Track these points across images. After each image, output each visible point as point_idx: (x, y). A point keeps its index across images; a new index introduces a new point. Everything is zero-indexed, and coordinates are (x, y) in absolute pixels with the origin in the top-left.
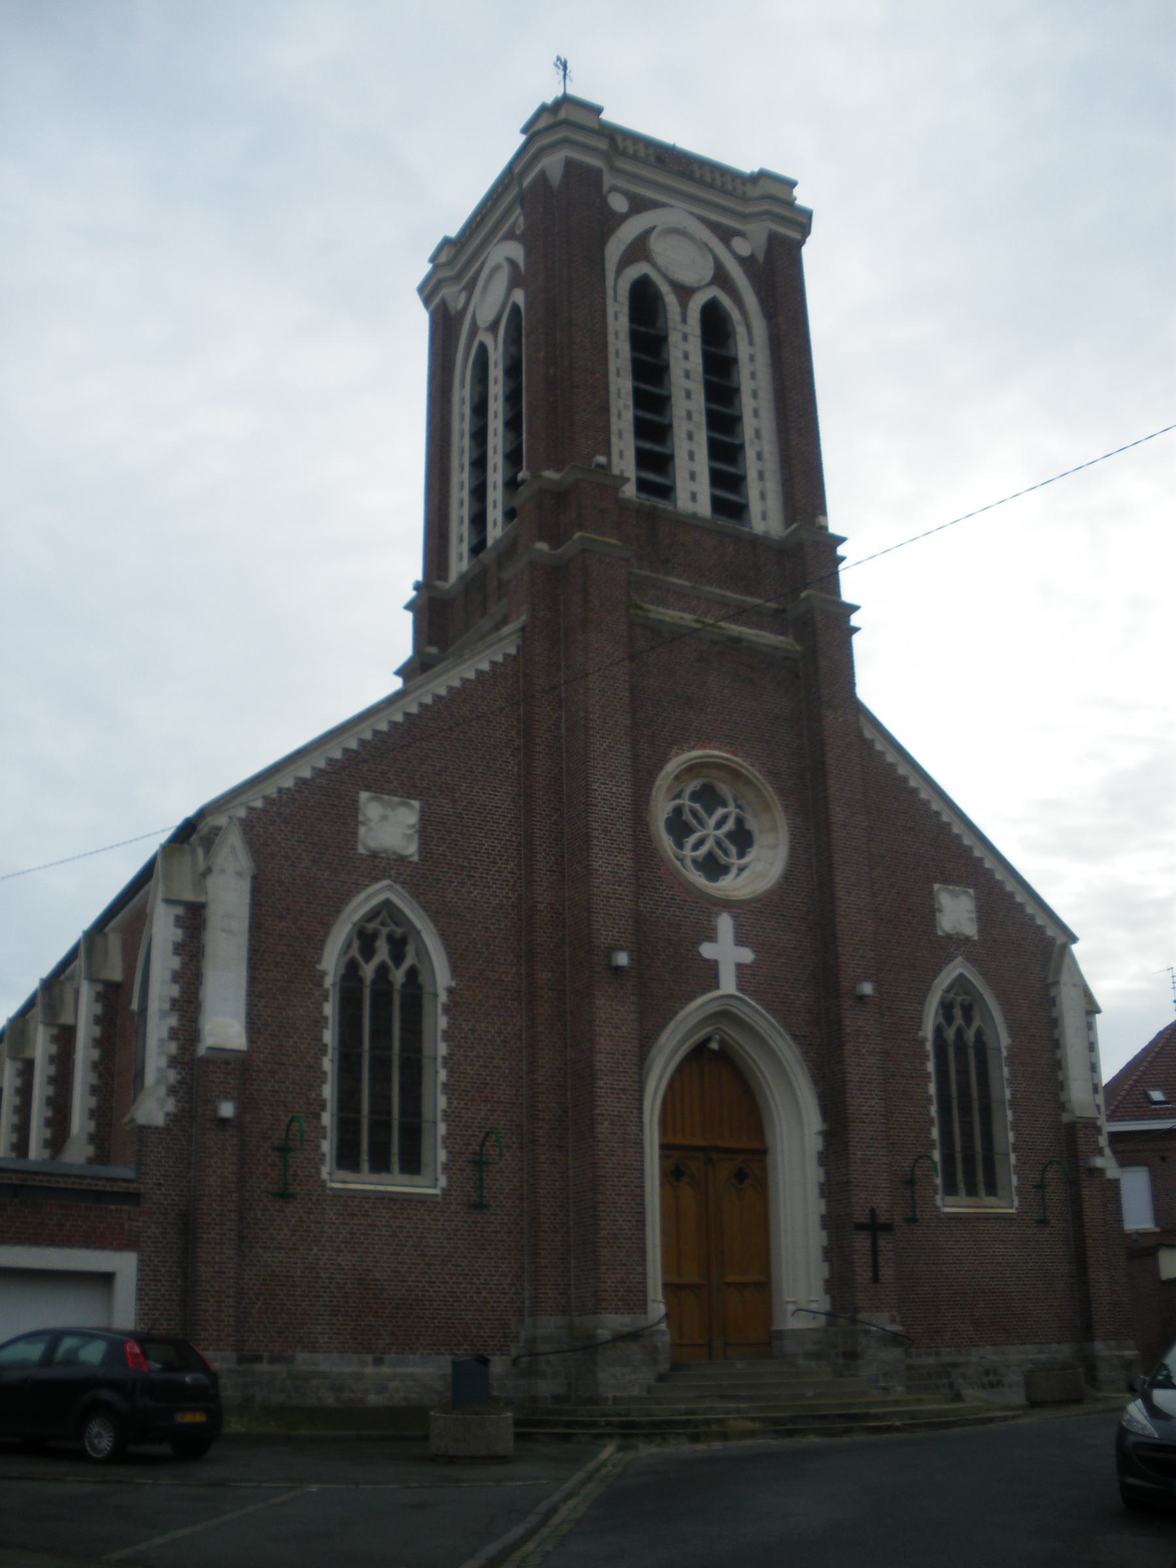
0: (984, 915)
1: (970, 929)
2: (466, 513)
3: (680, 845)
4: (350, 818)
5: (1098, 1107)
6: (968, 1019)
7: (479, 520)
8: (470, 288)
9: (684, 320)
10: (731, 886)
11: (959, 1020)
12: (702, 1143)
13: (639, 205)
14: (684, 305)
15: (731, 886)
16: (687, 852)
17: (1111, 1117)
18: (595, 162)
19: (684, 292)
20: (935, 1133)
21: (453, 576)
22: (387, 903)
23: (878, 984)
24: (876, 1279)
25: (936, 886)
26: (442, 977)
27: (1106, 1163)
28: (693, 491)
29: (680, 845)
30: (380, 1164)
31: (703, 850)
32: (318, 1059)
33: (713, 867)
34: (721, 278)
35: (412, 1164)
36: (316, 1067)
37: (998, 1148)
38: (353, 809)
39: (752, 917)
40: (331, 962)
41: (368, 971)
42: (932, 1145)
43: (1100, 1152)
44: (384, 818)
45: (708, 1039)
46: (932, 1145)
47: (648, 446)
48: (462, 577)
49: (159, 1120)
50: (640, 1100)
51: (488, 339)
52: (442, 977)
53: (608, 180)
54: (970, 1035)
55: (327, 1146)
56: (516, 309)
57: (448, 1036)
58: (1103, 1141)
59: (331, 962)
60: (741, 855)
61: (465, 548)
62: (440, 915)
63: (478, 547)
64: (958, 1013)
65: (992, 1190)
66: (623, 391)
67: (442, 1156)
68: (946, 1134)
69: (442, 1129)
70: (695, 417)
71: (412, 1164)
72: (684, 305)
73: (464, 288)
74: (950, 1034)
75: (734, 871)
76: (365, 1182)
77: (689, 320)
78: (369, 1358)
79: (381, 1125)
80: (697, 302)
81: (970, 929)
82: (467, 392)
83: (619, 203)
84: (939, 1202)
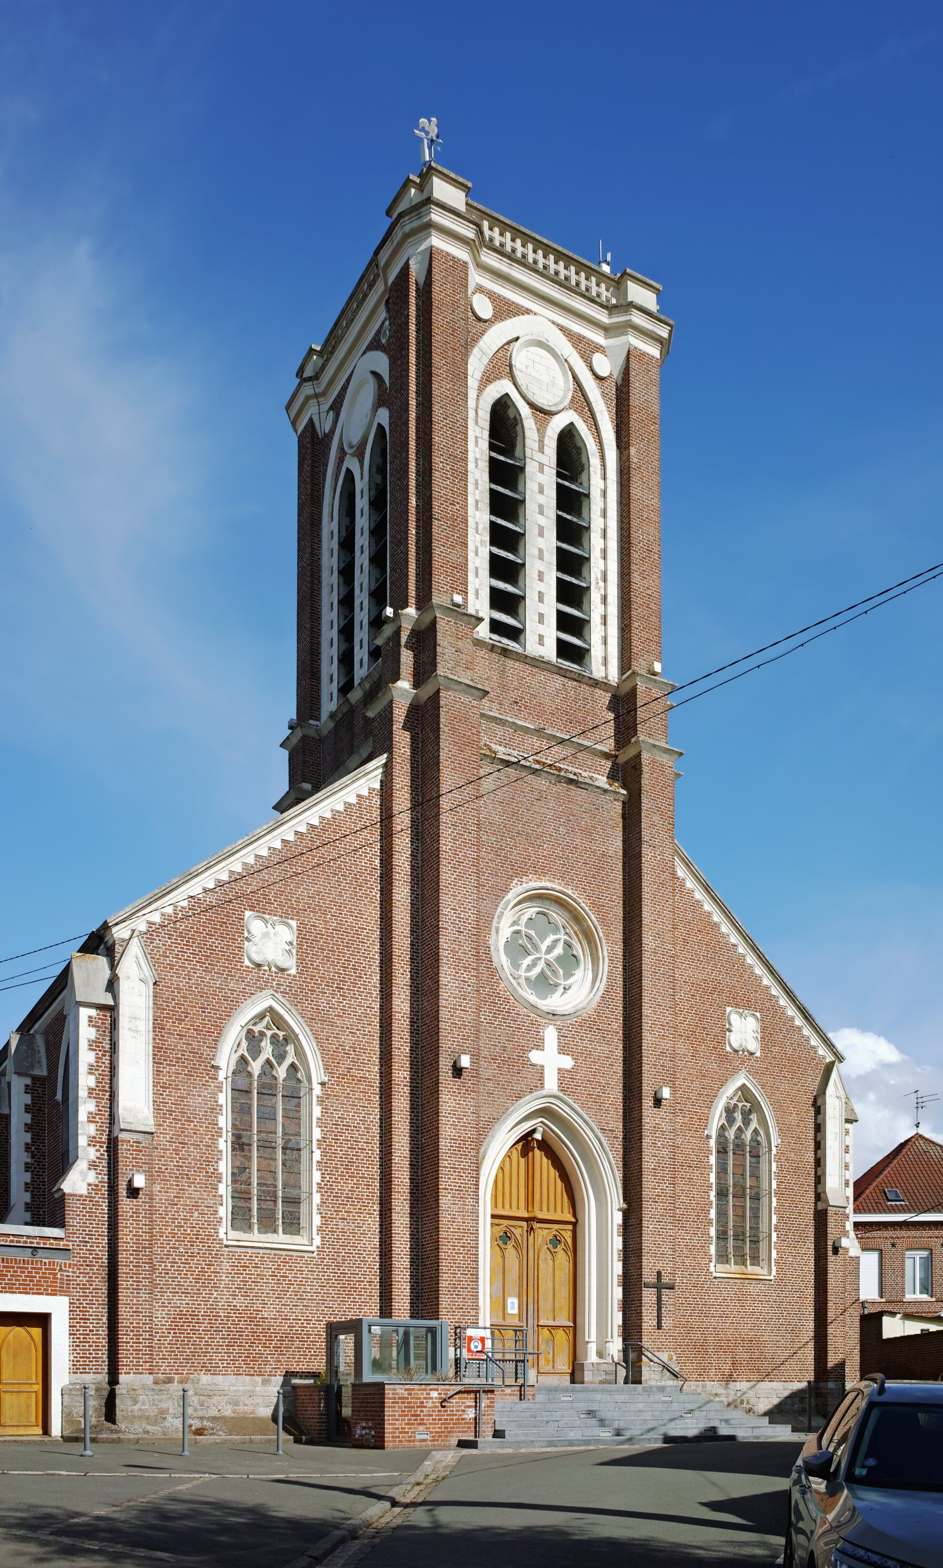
0: (767, 1035)
1: (753, 1046)
2: (334, 652)
3: (516, 965)
4: (235, 935)
5: (848, 1198)
6: (747, 1121)
7: (346, 659)
8: (336, 407)
9: (541, 450)
10: (556, 1002)
11: (739, 1123)
12: (526, 1215)
13: (504, 310)
14: (541, 431)
15: (556, 1002)
16: (522, 972)
17: (857, 1211)
18: (461, 253)
19: (543, 413)
20: (713, 1214)
21: (324, 715)
22: (271, 1009)
23: (674, 1091)
24: (659, 1326)
25: (728, 1009)
26: (317, 1073)
27: (850, 1243)
28: (541, 634)
29: (516, 965)
30: (267, 1224)
31: (537, 971)
32: (214, 1139)
33: (544, 984)
34: (581, 401)
35: (293, 1225)
36: (212, 1146)
37: (763, 1228)
38: (241, 926)
39: (574, 1034)
40: (225, 1059)
41: (256, 1067)
42: (710, 1223)
43: (846, 1234)
44: (266, 935)
45: (534, 1131)
46: (710, 1223)
47: (501, 585)
48: (332, 716)
49: (83, 1190)
50: (477, 1178)
51: (351, 463)
52: (317, 1073)
53: (476, 278)
54: (748, 1135)
55: (224, 1211)
56: (380, 427)
57: (321, 1123)
58: (849, 1226)
59: (225, 1059)
60: (568, 975)
61: (334, 688)
62: (313, 1019)
63: (346, 688)
64: (738, 1116)
65: (755, 1260)
66: (481, 527)
67: (317, 1220)
68: (722, 1213)
69: (317, 1198)
70: (546, 556)
71: (293, 1225)
72: (541, 431)
73: (331, 408)
74: (731, 1134)
75: (561, 989)
76: (256, 1238)
77: (546, 449)
78: (259, 1379)
79: (268, 1195)
80: (558, 424)
81: (753, 1046)
82: (335, 526)
83: (484, 308)
84: (712, 1269)
